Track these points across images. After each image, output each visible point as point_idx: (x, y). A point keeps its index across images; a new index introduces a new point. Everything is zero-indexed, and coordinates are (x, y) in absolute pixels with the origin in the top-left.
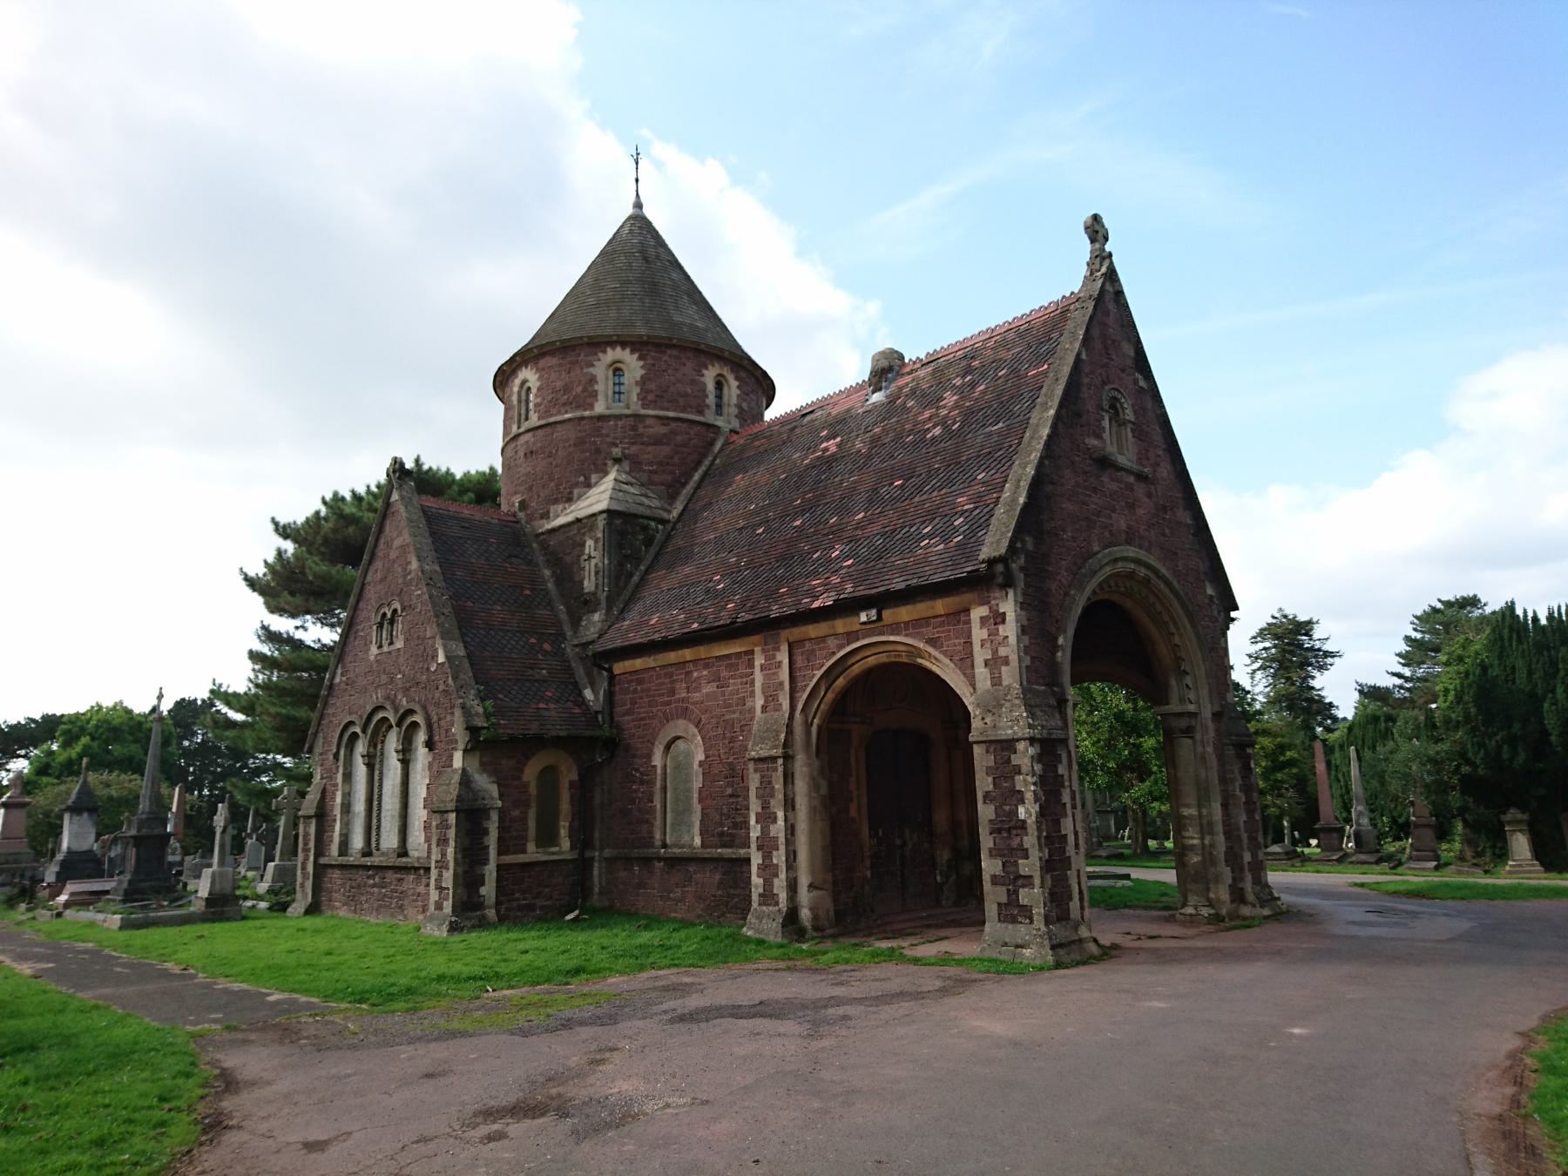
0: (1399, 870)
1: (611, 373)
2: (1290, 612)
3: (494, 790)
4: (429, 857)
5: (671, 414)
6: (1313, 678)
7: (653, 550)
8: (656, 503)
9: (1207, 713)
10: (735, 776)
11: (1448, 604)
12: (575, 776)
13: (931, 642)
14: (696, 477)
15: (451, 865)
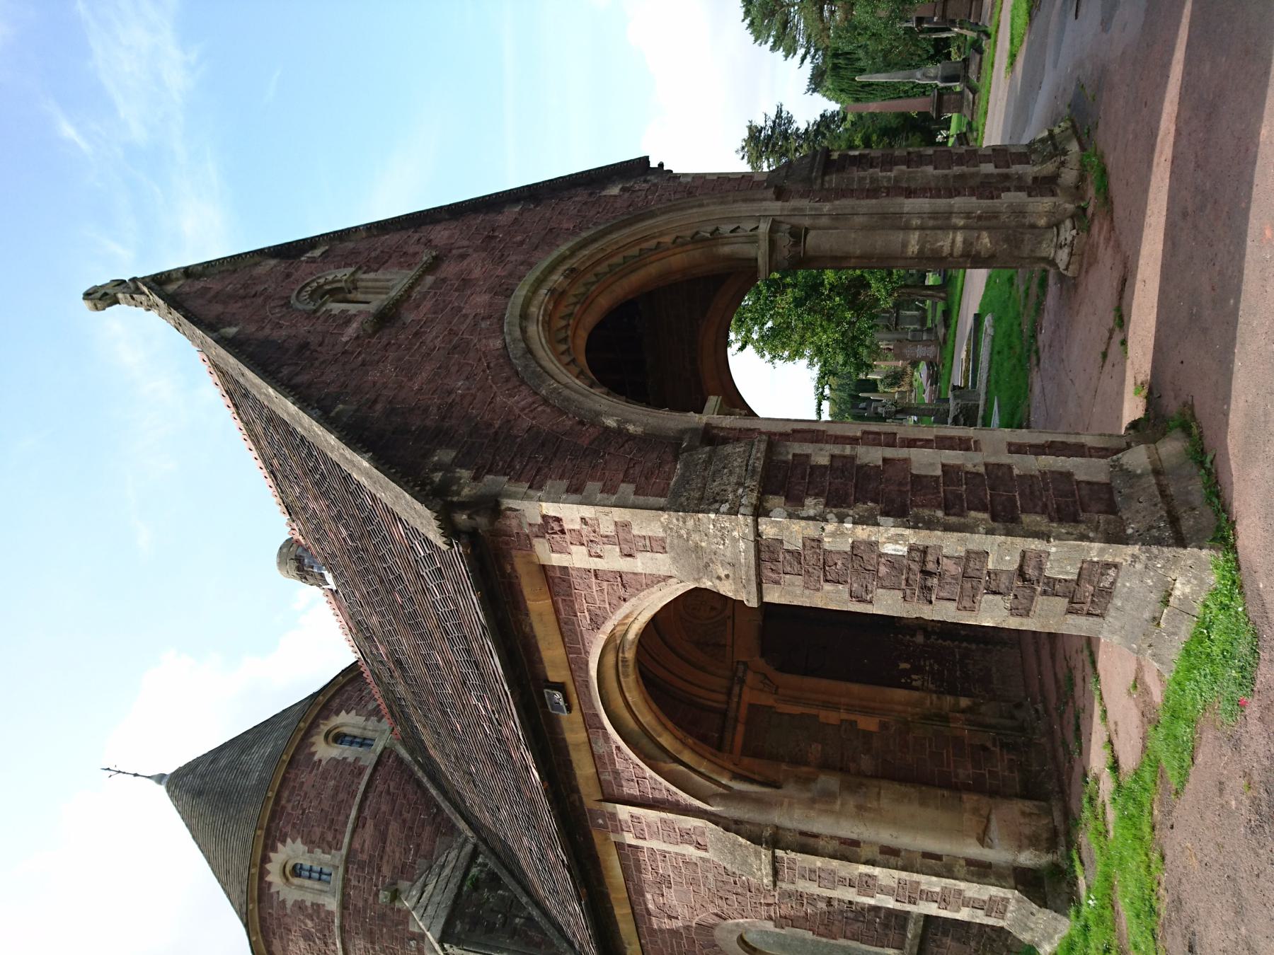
0: (991, 29)
1: (296, 881)
2: (740, 144)
6: (798, 129)
7: (506, 879)
9: (775, 207)
11: (747, 13)
13: (596, 624)
14: (434, 792)
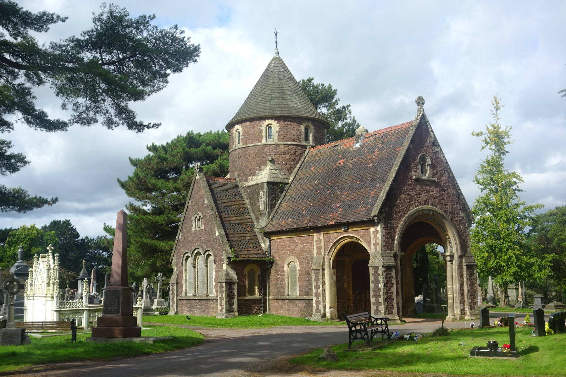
3: (235, 276)
4: (217, 296)
5: (289, 143)
8: (284, 176)
10: (308, 274)
12: (259, 273)
13: (362, 237)
14: (299, 165)
15: (225, 299)
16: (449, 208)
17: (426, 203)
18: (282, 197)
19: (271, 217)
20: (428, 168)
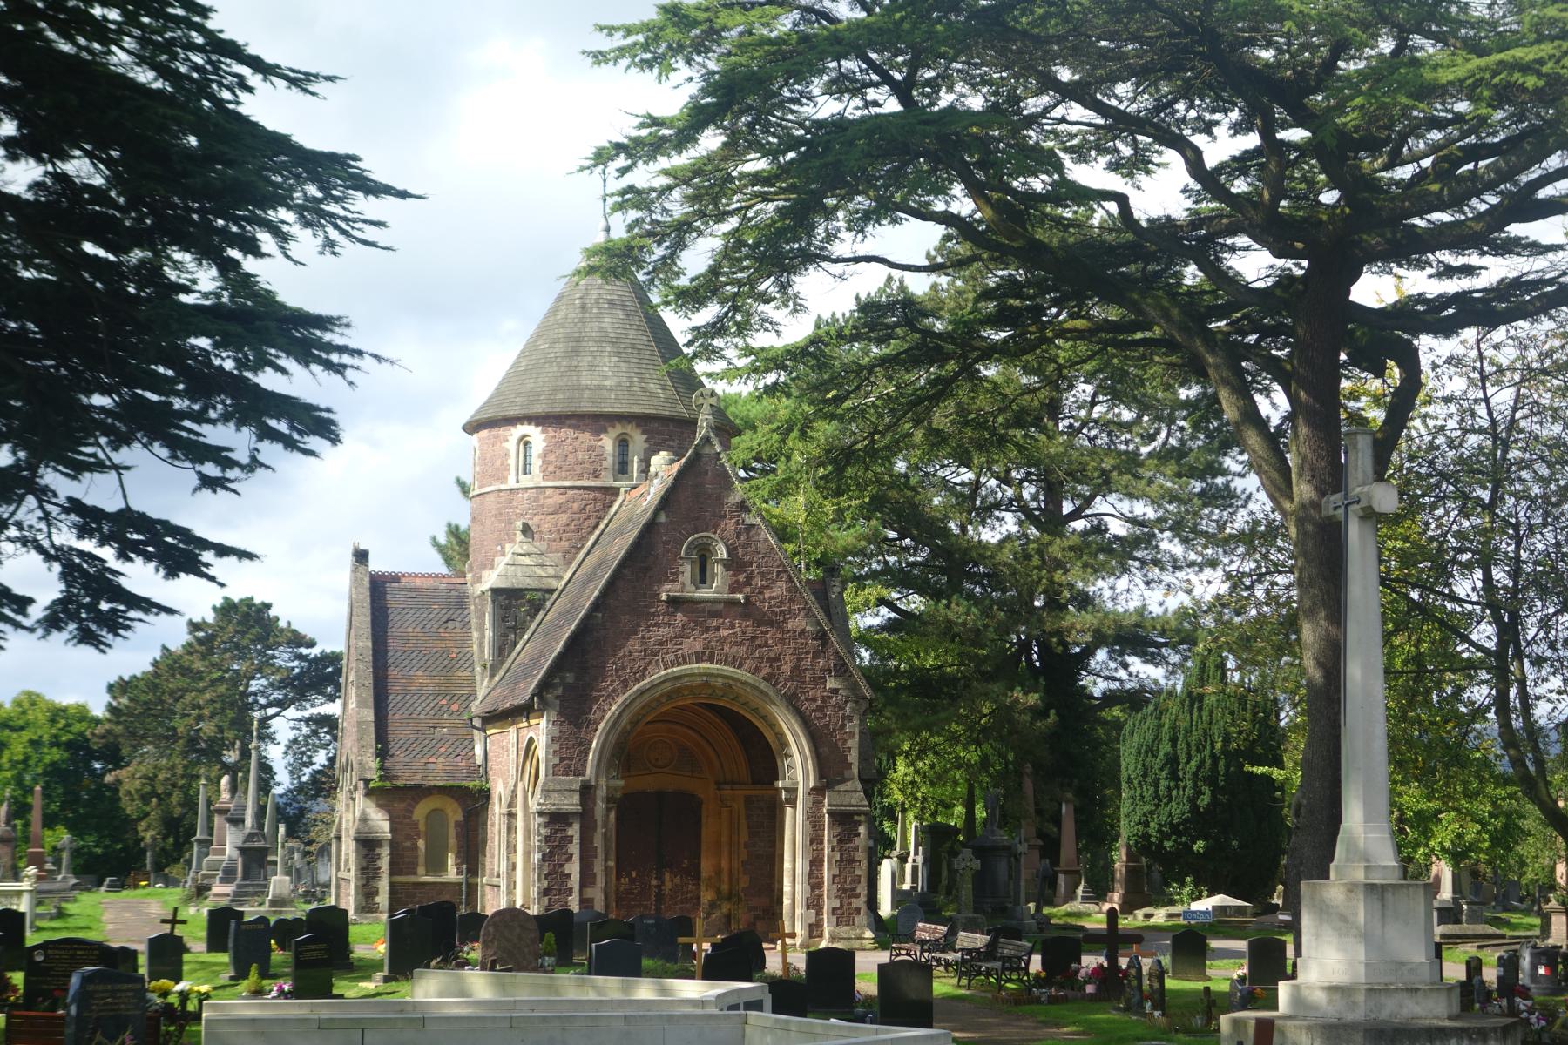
3: (386, 826)
5: (567, 483)
8: (551, 571)
12: (460, 817)
16: (786, 668)
17: (699, 657)
18: (533, 627)
19: (497, 679)
20: (718, 569)
